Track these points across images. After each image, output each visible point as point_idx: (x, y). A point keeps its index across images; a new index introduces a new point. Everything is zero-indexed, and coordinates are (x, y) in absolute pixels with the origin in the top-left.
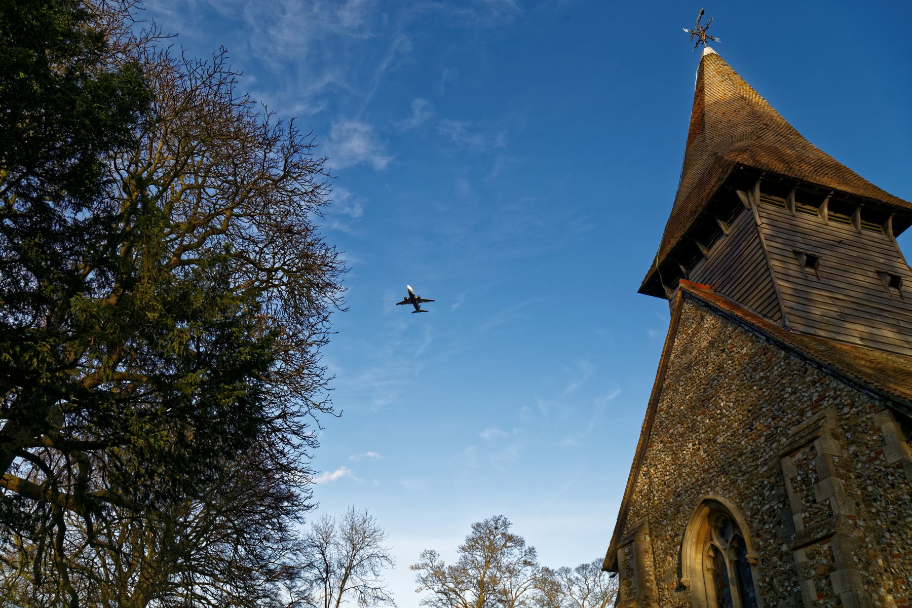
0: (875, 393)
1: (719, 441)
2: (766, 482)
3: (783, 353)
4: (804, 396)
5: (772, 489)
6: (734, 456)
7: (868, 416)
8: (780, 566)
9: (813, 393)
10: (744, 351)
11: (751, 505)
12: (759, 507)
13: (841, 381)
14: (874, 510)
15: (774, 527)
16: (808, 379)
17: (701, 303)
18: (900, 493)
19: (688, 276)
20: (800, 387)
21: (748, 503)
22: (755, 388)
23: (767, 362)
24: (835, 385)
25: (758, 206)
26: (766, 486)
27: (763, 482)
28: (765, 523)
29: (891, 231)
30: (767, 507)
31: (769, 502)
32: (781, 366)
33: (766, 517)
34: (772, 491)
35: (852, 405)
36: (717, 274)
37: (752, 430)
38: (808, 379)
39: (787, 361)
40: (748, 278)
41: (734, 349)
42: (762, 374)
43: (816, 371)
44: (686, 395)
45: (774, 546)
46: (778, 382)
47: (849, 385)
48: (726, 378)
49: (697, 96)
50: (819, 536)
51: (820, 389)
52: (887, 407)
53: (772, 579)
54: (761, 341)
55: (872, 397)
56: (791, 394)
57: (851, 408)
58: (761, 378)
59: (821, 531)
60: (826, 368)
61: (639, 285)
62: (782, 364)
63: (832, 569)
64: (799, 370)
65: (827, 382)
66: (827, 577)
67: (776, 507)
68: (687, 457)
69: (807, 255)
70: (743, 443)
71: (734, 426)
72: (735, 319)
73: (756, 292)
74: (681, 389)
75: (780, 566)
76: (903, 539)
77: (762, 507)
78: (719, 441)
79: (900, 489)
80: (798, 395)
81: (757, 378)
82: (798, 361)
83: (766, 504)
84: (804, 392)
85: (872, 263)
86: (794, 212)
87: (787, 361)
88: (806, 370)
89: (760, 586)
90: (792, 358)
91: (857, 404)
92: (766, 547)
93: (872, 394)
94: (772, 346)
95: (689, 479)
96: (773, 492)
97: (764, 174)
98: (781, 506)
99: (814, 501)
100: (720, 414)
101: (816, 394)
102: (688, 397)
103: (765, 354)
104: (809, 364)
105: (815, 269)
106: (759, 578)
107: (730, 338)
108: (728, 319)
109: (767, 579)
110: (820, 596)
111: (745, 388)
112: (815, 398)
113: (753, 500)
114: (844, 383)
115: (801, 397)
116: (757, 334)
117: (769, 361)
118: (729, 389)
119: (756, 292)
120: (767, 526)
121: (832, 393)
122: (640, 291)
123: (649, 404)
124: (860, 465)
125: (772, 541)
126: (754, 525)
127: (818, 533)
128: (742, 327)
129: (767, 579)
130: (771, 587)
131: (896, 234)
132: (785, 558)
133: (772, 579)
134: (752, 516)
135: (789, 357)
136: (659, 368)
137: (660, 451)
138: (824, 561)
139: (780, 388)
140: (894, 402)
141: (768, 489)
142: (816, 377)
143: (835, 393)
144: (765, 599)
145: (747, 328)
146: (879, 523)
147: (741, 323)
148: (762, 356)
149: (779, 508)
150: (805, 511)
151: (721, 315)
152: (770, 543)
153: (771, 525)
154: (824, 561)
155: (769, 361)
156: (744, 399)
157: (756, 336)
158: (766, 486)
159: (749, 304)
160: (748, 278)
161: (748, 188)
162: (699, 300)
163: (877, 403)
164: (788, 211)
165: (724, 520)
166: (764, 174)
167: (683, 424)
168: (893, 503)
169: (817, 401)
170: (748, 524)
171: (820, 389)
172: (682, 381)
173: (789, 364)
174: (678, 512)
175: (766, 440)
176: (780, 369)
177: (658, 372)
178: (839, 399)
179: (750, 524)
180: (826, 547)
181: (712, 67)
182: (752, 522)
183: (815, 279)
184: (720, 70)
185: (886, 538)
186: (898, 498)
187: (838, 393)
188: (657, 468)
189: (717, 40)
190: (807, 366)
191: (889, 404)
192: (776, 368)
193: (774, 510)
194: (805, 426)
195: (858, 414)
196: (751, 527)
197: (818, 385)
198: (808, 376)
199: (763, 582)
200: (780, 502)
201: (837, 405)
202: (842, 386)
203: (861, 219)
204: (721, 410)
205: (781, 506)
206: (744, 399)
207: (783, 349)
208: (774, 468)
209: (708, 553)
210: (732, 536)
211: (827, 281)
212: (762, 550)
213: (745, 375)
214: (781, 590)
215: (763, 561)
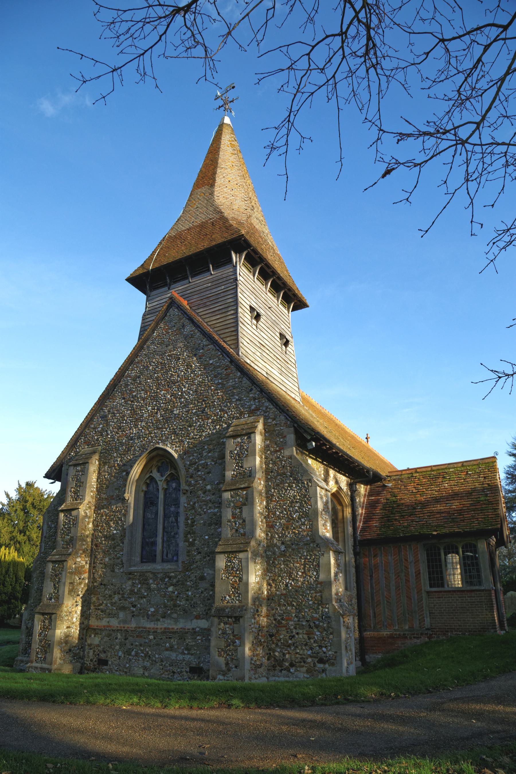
0: (290, 417)
1: (175, 412)
2: (206, 447)
3: (239, 374)
4: (246, 404)
5: (209, 452)
6: (185, 425)
7: (282, 428)
8: (203, 497)
9: (252, 404)
10: (211, 362)
11: (191, 458)
12: (197, 461)
13: (272, 404)
14: (269, 477)
15: (204, 474)
16: (251, 395)
17: (186, 316)
18: (286, 471)
19: (170, 285)
20: (245, 398)
21: (189, 457)
22: (212, 388)
23: (226, 375)
24: (268, 405)
25: (240, 267)
26: (205, 449)
27: (204, 447)
28: (198, 471)
29: (291, 309)
30: (203, 462)
31: (205, 459)
32: (235, 381)
33: (200, 468)
34: (209, 453)
35: (274, 419)
36: (196, 296)
37: (203, 413)
38: (251, 395)
39: (240, 380)
40: (220, 312)
41: (204, 358)
42: (220, 381)
43: (258, 393)
44: (155, 373)
45: (202, 485)
46: (230, 390)
47: (276, 408)
48: (191, 373)
49: (210, 152)
50: (242, 486)
51: (257, 404)
52: (294, 427)
53: (195, 503)
54: (226, 361)
55: (287, 418)
56: (237, 400)
57: (273, 420)
58: (219, 384)
59: (244, 484)
60: (265, 393)
61: (128, 275)
62: (236, 380)
63: (245, 504)
64: (247, 388)
65: (263, 401)
66: (240, 508)
67: (209, 463)
68: (145, 415)
69: (257, 313)
70: (194, 419)
71: (190, 406)
72: (210, 338)
73: (224, 323)
74: (151, 368)
75: (203, 497)
76: (279, 494)
77: (199, 461)
78: (175, 412)
79: (287, 469)
80: (242, 402)
81: (216, 382)
82: (248, 382)
83: (202, 460)
84: (247, 402)
85: (279, 327)
86: (255, 279)
87: (240, 380)
88: (252, 390)
89: (185, 506)
90: (244, 379)
91: (277, 420)
92: (195, 485)
93: (288, 417)
94: (232, 366)
95: (143, 431)
96: (210, 454)
97: (252, 248)
98: (213, 463)
99: (242, 467)
100: (180, 395)
101: (254, 406)
102: (156, 375)
103: (226, 370)
104: (255, 387)
105: (257, 322)
106: (185, 501)
107: (203, 349)
108: (205, 337)
109: (191, 503)
110: (234, 517)
111: (205, 385)
112: (253, 407)
113: (193, 456)
114: (273, 405)
115: (244, 404)
116: (224, 355)
117: (228, 375)
118: (193, 382)
119: (224, 323)
120: (199, 473)
121: (264, 409)
122: (127, 280)
123: (120, 369)
124: (269, 452)
125: (201, 482)
126: (191, 471)
127: (241, 484)
128: (214, 346)
129: (191, 503)
130: (193, 507)
131: (293, 310)
132: (207, 493)
133: (195, 503)
134: (191, 465)
135: (243, 378)
136: (136, 346)
137: (121, 404)
138: (241, 500)
139: (231, 395)
140: (298, 425)
141: (207, 452)
142: (257, 396)
143: (267, 409)
144: (187, 514)
145: (217, 348)
146: (270, 484)
147: (214, 343)
148: (224, 370)
149: (211, 464)
150: (234, 471)
151: (200, 331)
152: (199, 483)
153: (203, 473)
154: (241, 500)
155: (228, 375)
156: (202, 392)
157: (223, 356)
158: (205, 449)
159: (216, 329)
160: (220, 312)
161: (239, 252)
162: (185, 313)
163: (289, 422)
164: (252, 277)
165: (163, 462)
166: (252, 248)
167: (147, 392)
168: (281, 475)
169: (253, 410)
170: (186, 469)
171: (257, 404)
172: (154, 363)
173: (241, 381)
174: (129, 450)
175: (211, 423)
176: (234, 383)
177: (134, 348)
178: (268, 413)
179: (187, 471)
180: (245, 492)
181: (228, 137)
182: (189, 468)
183: (254, 327)
184: (233, 143)
185: (271, 492)
186: (284, 473)
187: (268, 410)
188: (115, 416)
189: (233, 114)
190: (253, 387)
191: (296, 425)
192: (231, 381)
193: (207, 465)
194: (244, 423)
195: (276, 425)
196: (187, 471)
197: (257, 401)
198: (252, 393)
199: (188, 504)
200: (213, 461)
201: (266, 416)
202: (272, 407)
203: (282, 298)
204: (182, 393)
205: (213, 463)
206: (202, 392)
207: (239, 371)
208: (214, 440)
209: (146, 480)
210: (169, 473)
211: (260, 332)
212: (192, 486)
213: (207, 377)
214: (200, 510)
215: (191, 492)
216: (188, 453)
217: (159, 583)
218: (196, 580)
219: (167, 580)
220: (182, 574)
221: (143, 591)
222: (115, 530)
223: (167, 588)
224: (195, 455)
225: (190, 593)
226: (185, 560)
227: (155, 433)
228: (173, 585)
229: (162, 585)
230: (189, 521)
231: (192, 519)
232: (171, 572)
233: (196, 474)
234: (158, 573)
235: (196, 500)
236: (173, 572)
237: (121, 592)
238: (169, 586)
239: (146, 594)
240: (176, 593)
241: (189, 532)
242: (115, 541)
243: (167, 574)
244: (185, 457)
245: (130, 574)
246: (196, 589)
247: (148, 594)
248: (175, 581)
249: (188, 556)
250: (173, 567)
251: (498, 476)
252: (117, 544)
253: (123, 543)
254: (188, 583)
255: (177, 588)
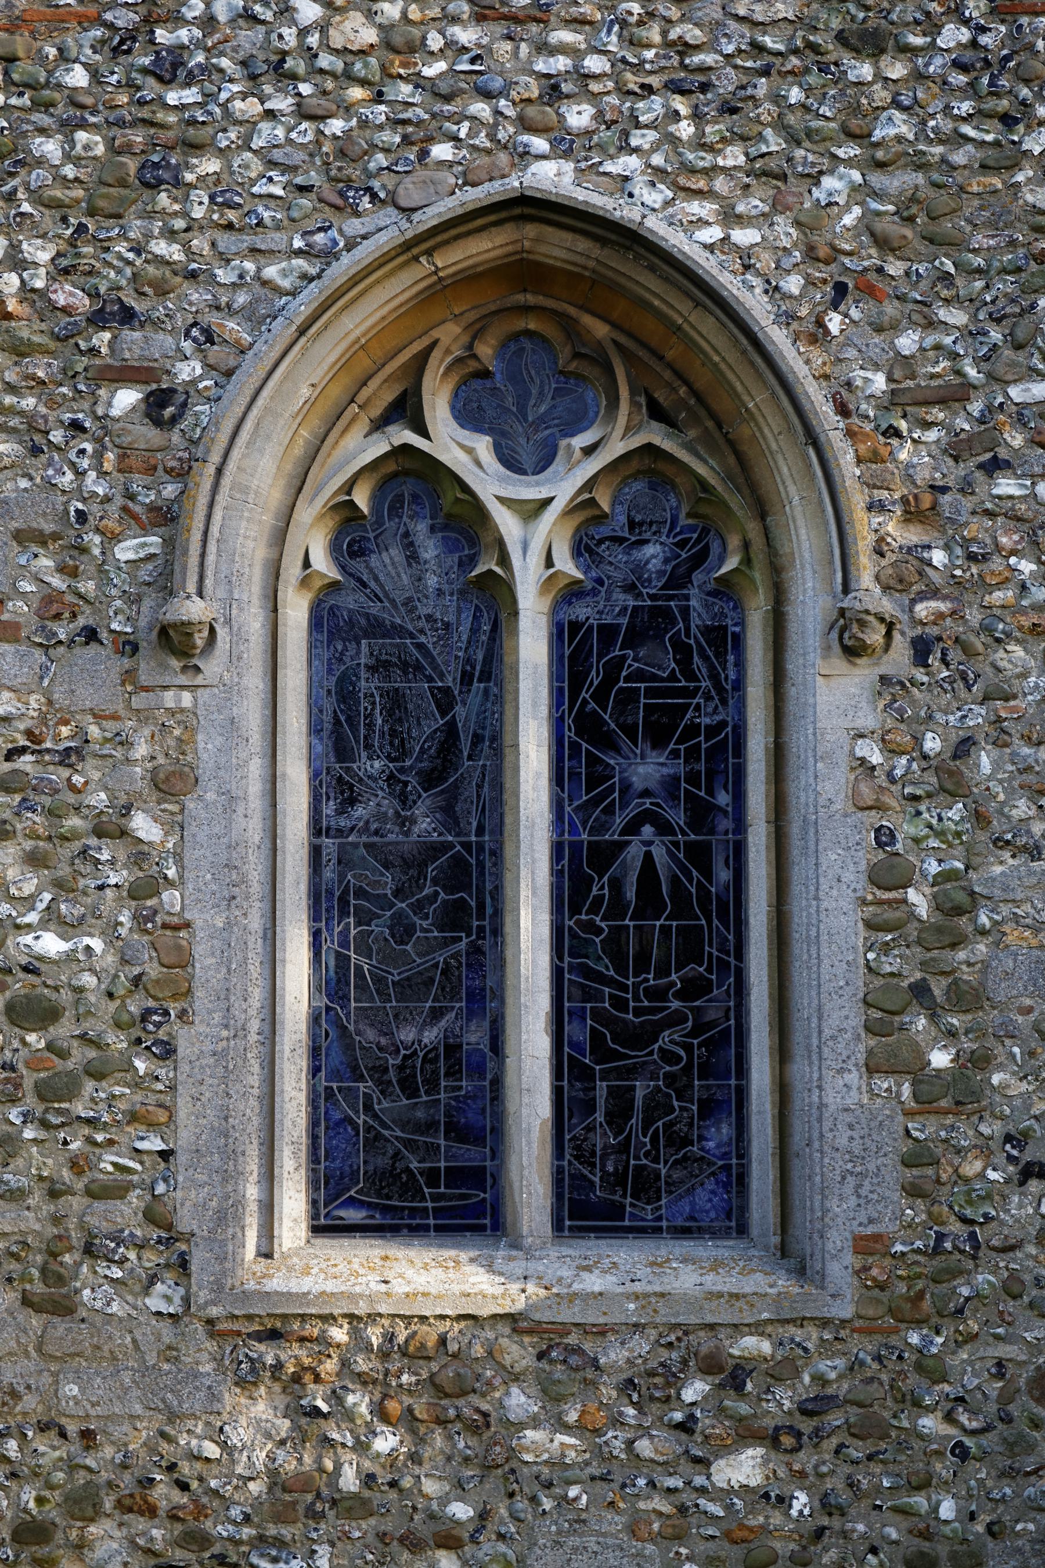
28: (994, 466)
53: (964, 747)
113: (931, 324)
129: (932, 744)
133: (964, 747)
199: (892, 751)
210: (617, 448)
216: (869, 291)
217: (618, 1422)
218: (1006, 1398)
219: (694, 1390)
220: (863, 1348)
221: (430, 1487)
222: (52, 919)
223: (703, 1463)
224: (956, 317)
225: (947, 1510)
226: (887, 1228)
227: (454, 49)
228: (771, 1440)
229: (644, 1431)
230: (918, 899)
231: (947, 876)
232: (738, 1329)
233: (966, 488)
234: (602, 1332)
235: (978, 716)
236: (757, 1328)
237: (164, 1494)
238: (726, 1449)
239: (461, 1511)
240: (801, 1501)
241: (920, 991)
242: (64, 1030)
243: (703, 1341)
244: (834, 323)
245: (273, 1335)
246: (1008, 1474)
247: (483, 1516)
248: (785, 1398)
249: (913, 1191)
250: (756, 1283)
251: (810, 727)
252: (80, 1055)
253: (167, 1052)
254: (929, 1423)
255: (805, 1460)
